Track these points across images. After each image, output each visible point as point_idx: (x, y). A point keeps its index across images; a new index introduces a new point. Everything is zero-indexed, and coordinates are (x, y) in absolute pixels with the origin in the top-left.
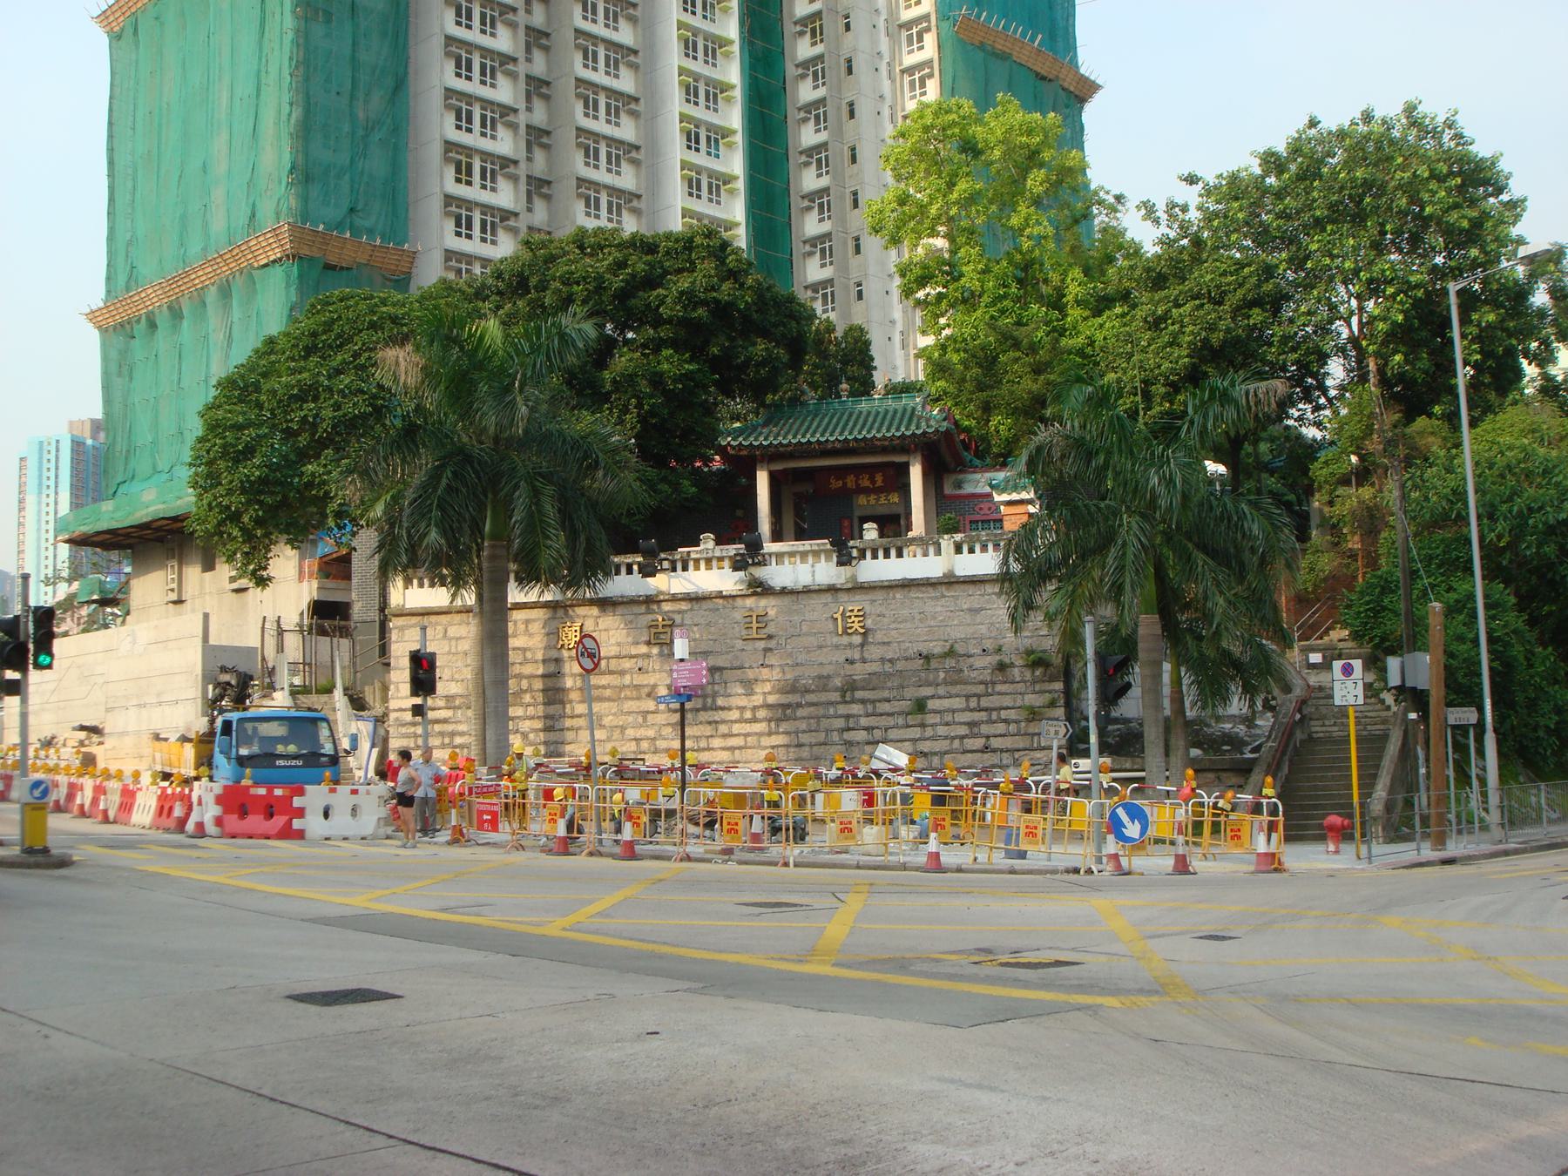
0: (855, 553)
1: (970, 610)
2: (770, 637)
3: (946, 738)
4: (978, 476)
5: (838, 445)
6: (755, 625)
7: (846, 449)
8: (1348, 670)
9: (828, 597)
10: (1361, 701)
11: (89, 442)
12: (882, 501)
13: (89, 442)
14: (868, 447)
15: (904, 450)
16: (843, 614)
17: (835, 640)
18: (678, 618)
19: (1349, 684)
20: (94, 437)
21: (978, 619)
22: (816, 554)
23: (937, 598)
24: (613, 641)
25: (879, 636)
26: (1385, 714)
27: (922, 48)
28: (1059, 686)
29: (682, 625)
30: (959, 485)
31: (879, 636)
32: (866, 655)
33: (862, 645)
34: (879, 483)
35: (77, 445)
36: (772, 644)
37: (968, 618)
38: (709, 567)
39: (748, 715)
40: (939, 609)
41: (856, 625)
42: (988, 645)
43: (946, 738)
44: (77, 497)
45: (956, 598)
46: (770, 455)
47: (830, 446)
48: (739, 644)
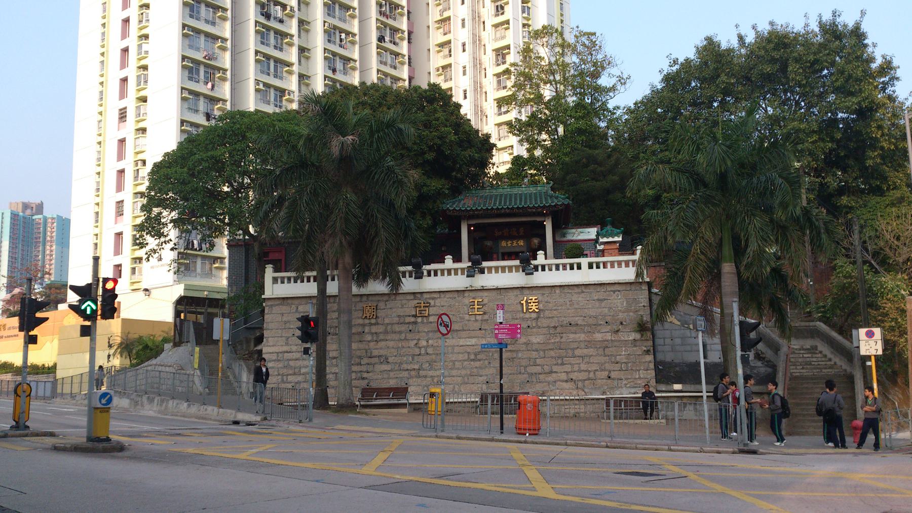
0: (425, 273)
1: (598, 300)
2: (485, 313)
3: (586, 371)
4: (574, 231)
5: (508, 211)
6: (476, 307)
7: (512, 213)
8: (870, 335)
9: (517, 292)
10: (880, 352)
11: (21, 214)
12: (515, 244)
13: (21, 214)
14: (524, 211)
15: (541, 214)
16: (526, 301)
17: (522, 315)
18: (432, 302)
19: (872, 342)
20: (23, 212)
21: (603, 304)
22: (510, 269)
23: (579, 293)
24: (395, 314)
25: (547, 313)
26: (829, 363)
27: (503, 14)
28: (650, 343)
29: (434, 306)
30: (564, 235)
31: (547, 313)
32: (539, 324)
33: (537, 319)
34: (521, 234)
35: (14, 216)
36: (486, 317)
37: (597, 304)
38: (497, 272)
39: (472, 357)
40: (580, 299)
41: (534, 308)
42: (608, 319)
43: (586, 371)
44: (13, 244)
45: (591, 293)
46: (470, 215)
47: (503, 211)
48: (467, 317)
